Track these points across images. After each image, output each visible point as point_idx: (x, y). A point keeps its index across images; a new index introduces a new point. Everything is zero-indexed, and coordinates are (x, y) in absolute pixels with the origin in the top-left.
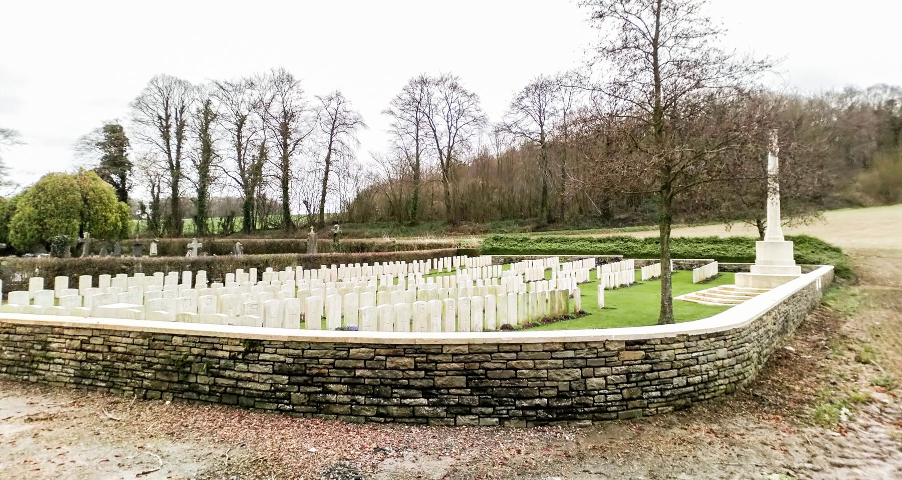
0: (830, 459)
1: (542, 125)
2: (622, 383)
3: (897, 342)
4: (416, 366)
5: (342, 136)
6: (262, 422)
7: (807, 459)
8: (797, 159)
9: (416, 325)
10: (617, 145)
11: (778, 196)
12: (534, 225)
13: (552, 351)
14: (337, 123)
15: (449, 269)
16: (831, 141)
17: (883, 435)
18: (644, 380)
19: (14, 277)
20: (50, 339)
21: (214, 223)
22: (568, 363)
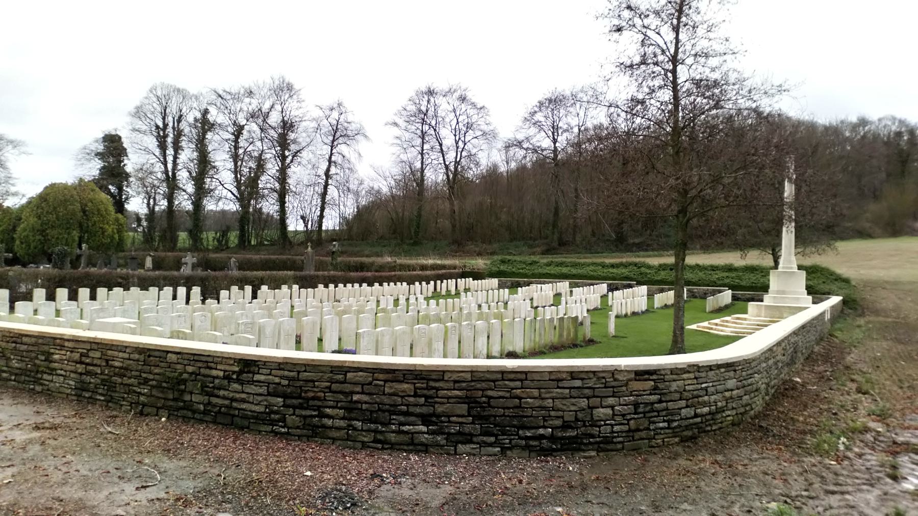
0: (825, 487)
1: (555, 141)
2: (630, 414)
3: (894, 373)
4: (415, 392)
5: (342, 148)
6: (257, 444)
7: (804, 487)
8: (813, 187)
9: (417, 349)
10: (633, 166)
11: (793, 224)
12: (544, 248)
13: (558, 380)
14: (338, 134)
15: (453, 292)
16: (844, 170)
17: (874, 463)
18: (652, 411)
19: (20, 287)
20: (52, 351)
21: (209, 237)
22: (574, 393)
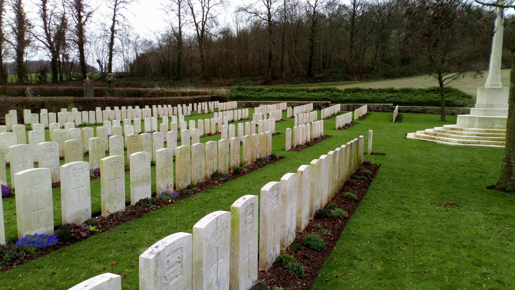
12: (263, 81)
15: (206, 111)
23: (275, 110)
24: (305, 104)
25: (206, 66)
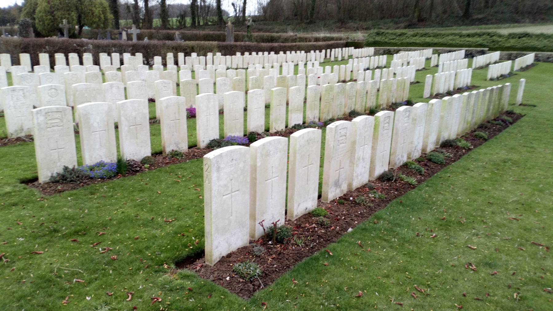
12: (407, 24)
15: (340, 59)
23: (417, 57)
24: (455, 51)
25: (342, 7)
